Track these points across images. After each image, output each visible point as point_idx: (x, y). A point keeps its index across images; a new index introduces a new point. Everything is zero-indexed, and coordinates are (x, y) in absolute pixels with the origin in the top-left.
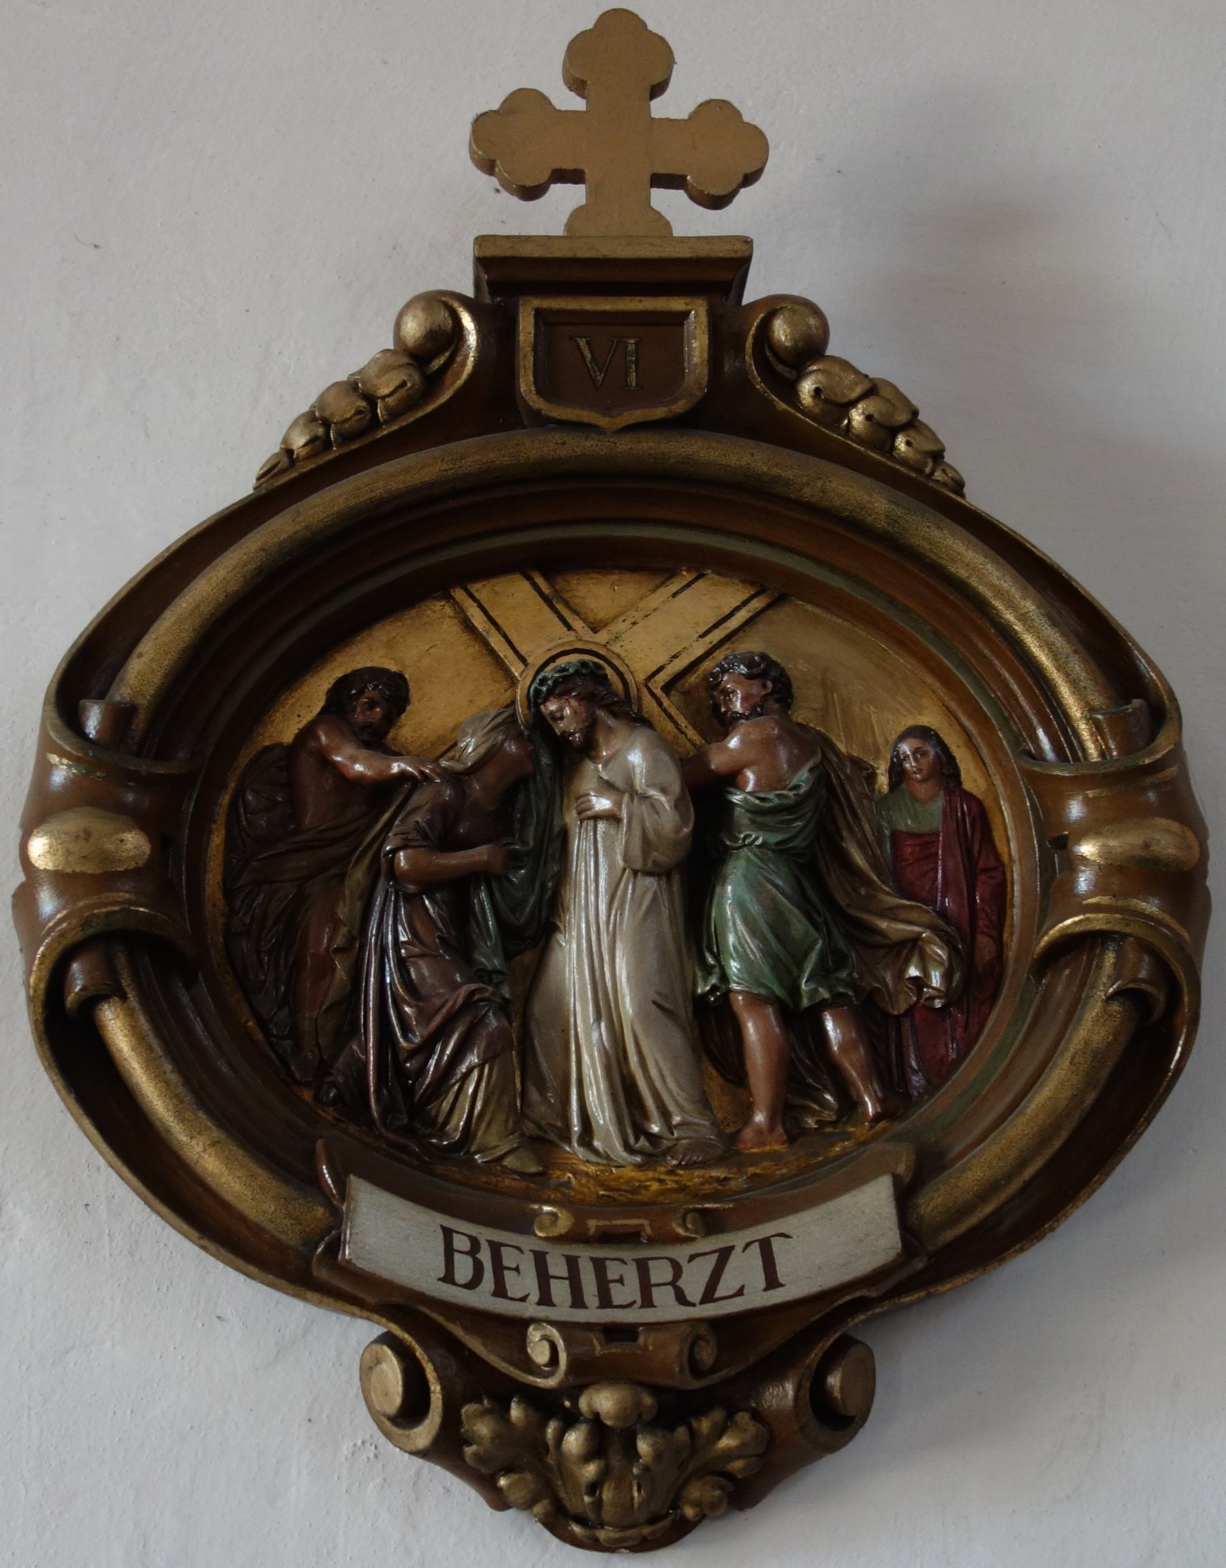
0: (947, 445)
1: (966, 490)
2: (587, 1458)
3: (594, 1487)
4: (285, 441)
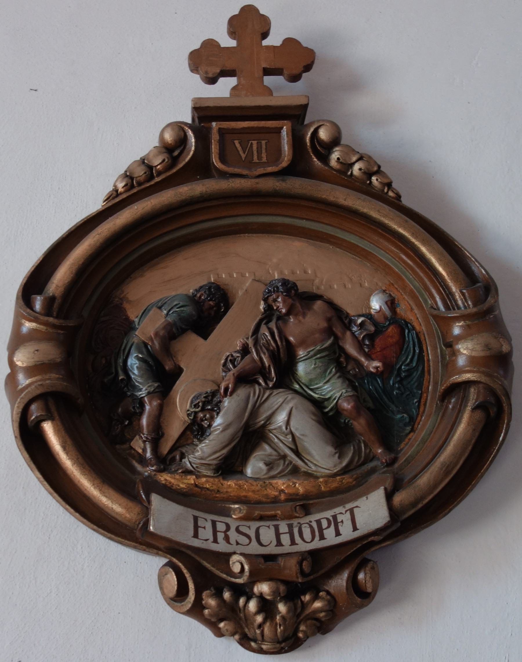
1: (402, 199)
2: (258, 612)
3: (260, 626)
4: (115, 186)
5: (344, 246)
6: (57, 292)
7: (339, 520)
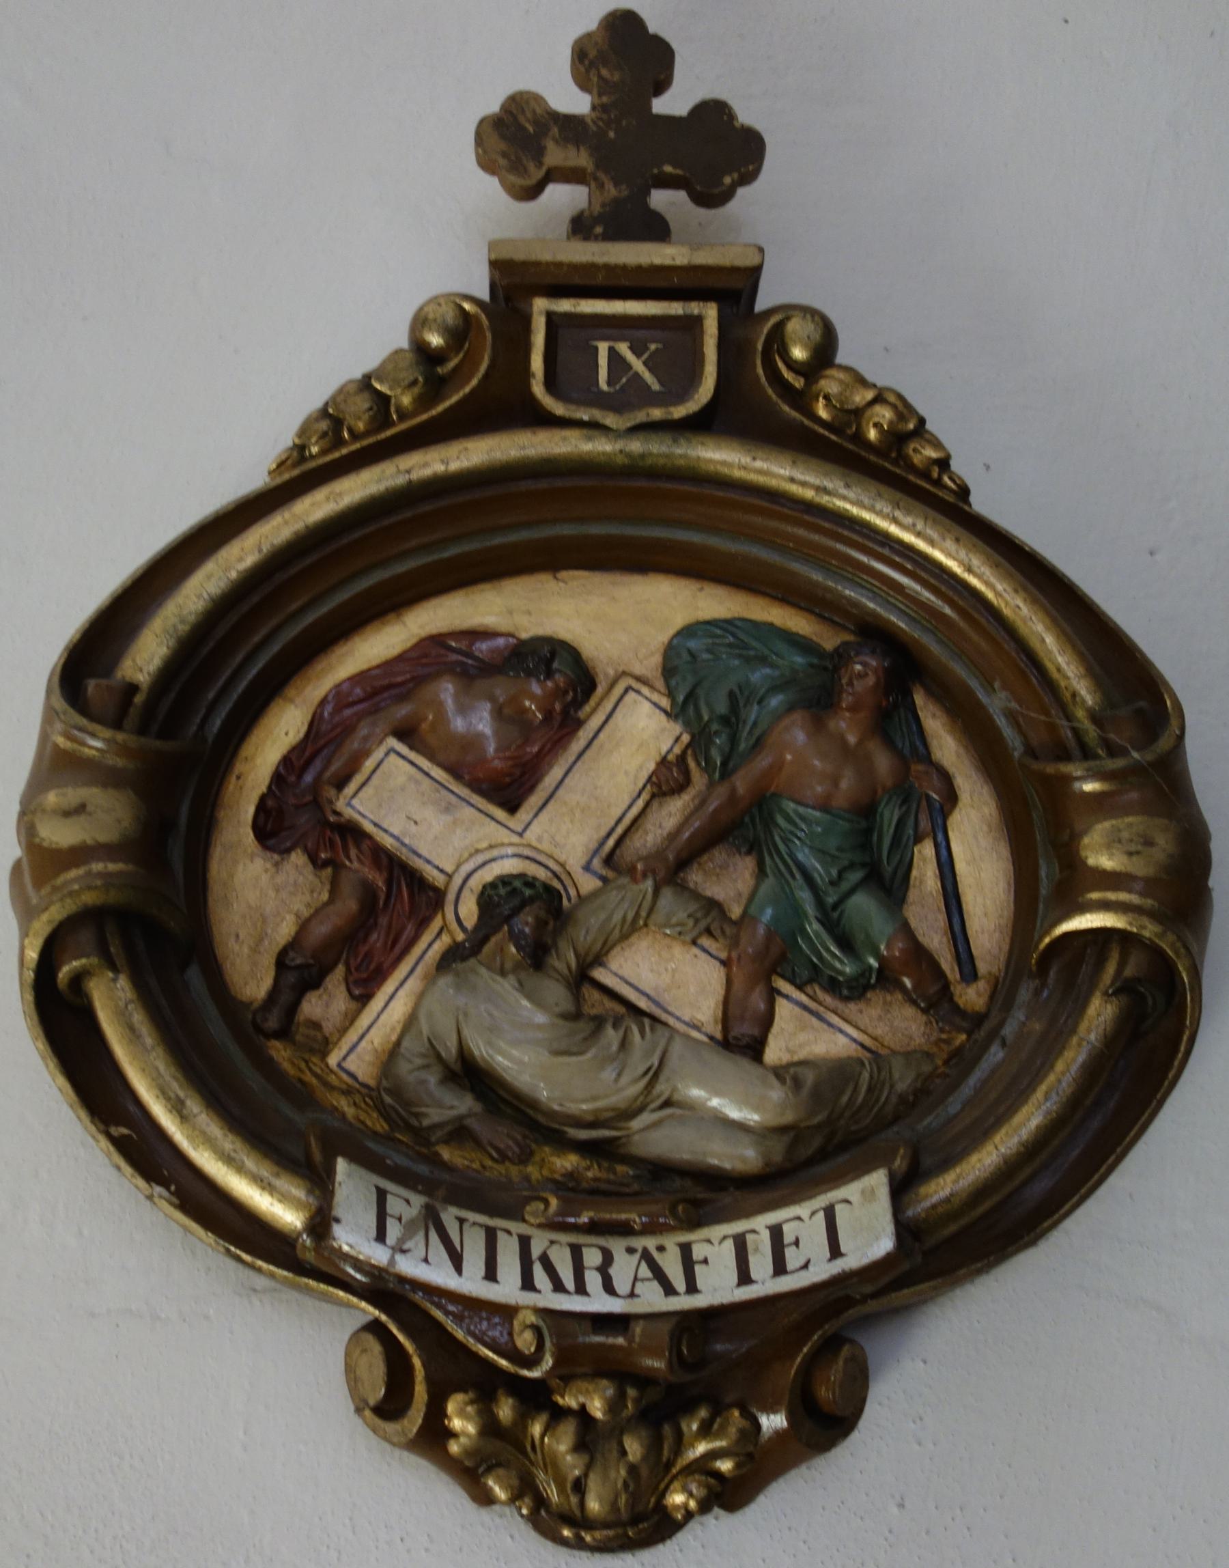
0: (952, 453)
5: (834, 565)
6: (505, 1131)
7: (788, 1238)
